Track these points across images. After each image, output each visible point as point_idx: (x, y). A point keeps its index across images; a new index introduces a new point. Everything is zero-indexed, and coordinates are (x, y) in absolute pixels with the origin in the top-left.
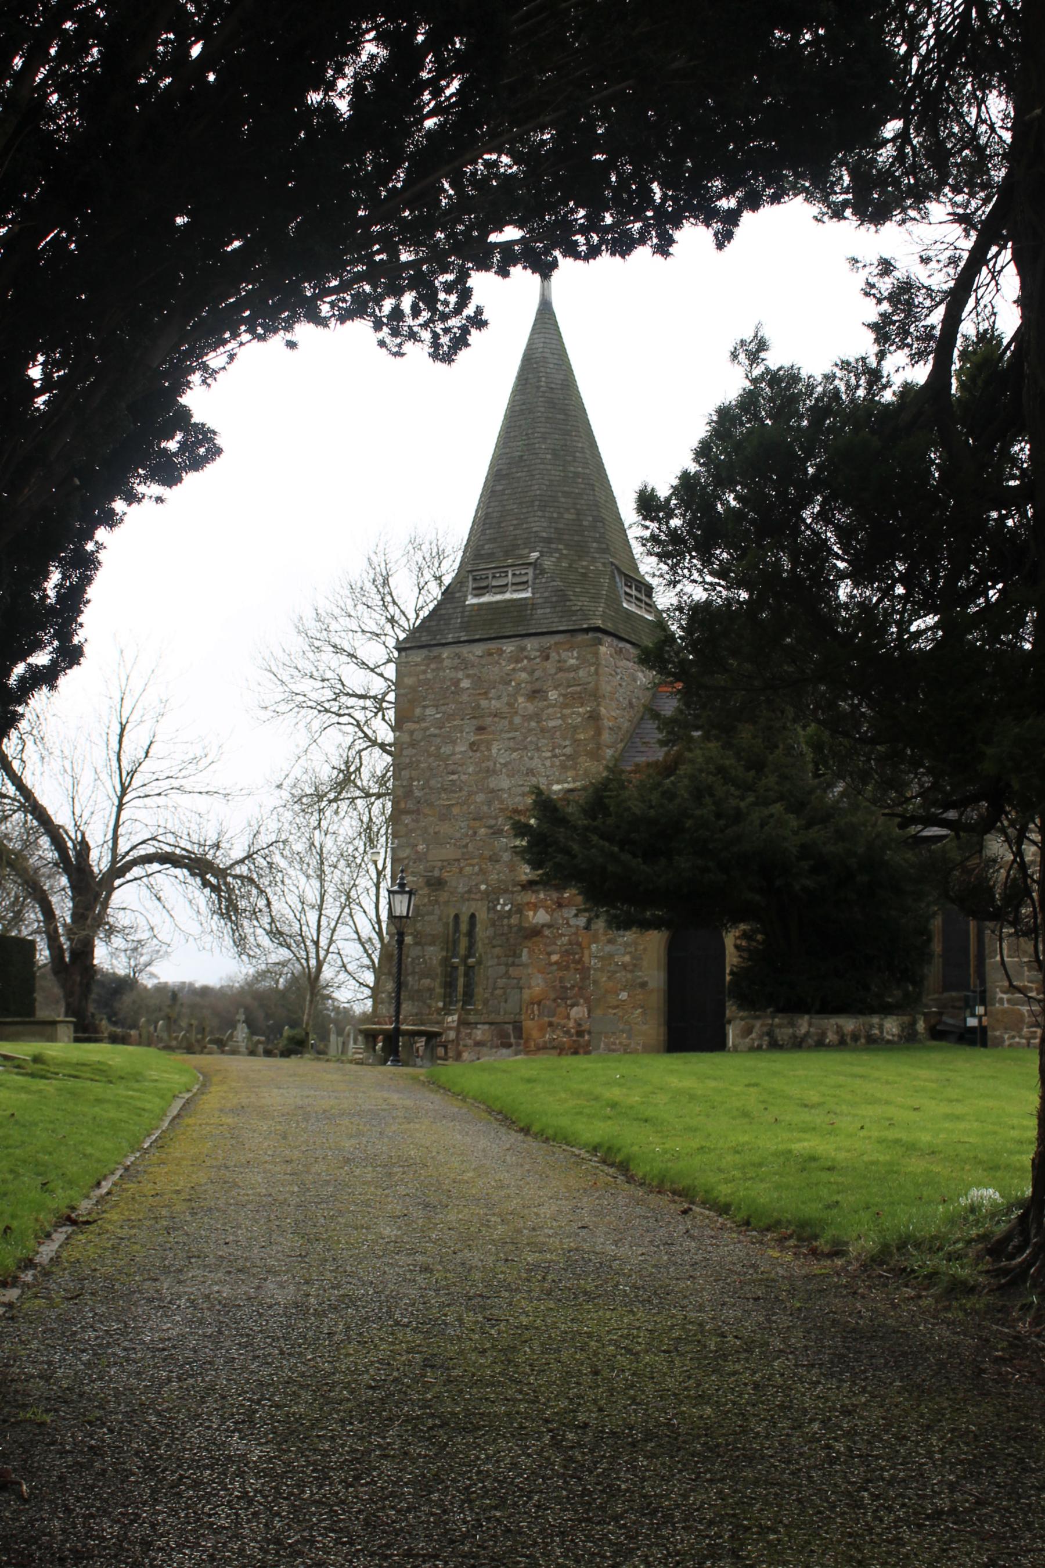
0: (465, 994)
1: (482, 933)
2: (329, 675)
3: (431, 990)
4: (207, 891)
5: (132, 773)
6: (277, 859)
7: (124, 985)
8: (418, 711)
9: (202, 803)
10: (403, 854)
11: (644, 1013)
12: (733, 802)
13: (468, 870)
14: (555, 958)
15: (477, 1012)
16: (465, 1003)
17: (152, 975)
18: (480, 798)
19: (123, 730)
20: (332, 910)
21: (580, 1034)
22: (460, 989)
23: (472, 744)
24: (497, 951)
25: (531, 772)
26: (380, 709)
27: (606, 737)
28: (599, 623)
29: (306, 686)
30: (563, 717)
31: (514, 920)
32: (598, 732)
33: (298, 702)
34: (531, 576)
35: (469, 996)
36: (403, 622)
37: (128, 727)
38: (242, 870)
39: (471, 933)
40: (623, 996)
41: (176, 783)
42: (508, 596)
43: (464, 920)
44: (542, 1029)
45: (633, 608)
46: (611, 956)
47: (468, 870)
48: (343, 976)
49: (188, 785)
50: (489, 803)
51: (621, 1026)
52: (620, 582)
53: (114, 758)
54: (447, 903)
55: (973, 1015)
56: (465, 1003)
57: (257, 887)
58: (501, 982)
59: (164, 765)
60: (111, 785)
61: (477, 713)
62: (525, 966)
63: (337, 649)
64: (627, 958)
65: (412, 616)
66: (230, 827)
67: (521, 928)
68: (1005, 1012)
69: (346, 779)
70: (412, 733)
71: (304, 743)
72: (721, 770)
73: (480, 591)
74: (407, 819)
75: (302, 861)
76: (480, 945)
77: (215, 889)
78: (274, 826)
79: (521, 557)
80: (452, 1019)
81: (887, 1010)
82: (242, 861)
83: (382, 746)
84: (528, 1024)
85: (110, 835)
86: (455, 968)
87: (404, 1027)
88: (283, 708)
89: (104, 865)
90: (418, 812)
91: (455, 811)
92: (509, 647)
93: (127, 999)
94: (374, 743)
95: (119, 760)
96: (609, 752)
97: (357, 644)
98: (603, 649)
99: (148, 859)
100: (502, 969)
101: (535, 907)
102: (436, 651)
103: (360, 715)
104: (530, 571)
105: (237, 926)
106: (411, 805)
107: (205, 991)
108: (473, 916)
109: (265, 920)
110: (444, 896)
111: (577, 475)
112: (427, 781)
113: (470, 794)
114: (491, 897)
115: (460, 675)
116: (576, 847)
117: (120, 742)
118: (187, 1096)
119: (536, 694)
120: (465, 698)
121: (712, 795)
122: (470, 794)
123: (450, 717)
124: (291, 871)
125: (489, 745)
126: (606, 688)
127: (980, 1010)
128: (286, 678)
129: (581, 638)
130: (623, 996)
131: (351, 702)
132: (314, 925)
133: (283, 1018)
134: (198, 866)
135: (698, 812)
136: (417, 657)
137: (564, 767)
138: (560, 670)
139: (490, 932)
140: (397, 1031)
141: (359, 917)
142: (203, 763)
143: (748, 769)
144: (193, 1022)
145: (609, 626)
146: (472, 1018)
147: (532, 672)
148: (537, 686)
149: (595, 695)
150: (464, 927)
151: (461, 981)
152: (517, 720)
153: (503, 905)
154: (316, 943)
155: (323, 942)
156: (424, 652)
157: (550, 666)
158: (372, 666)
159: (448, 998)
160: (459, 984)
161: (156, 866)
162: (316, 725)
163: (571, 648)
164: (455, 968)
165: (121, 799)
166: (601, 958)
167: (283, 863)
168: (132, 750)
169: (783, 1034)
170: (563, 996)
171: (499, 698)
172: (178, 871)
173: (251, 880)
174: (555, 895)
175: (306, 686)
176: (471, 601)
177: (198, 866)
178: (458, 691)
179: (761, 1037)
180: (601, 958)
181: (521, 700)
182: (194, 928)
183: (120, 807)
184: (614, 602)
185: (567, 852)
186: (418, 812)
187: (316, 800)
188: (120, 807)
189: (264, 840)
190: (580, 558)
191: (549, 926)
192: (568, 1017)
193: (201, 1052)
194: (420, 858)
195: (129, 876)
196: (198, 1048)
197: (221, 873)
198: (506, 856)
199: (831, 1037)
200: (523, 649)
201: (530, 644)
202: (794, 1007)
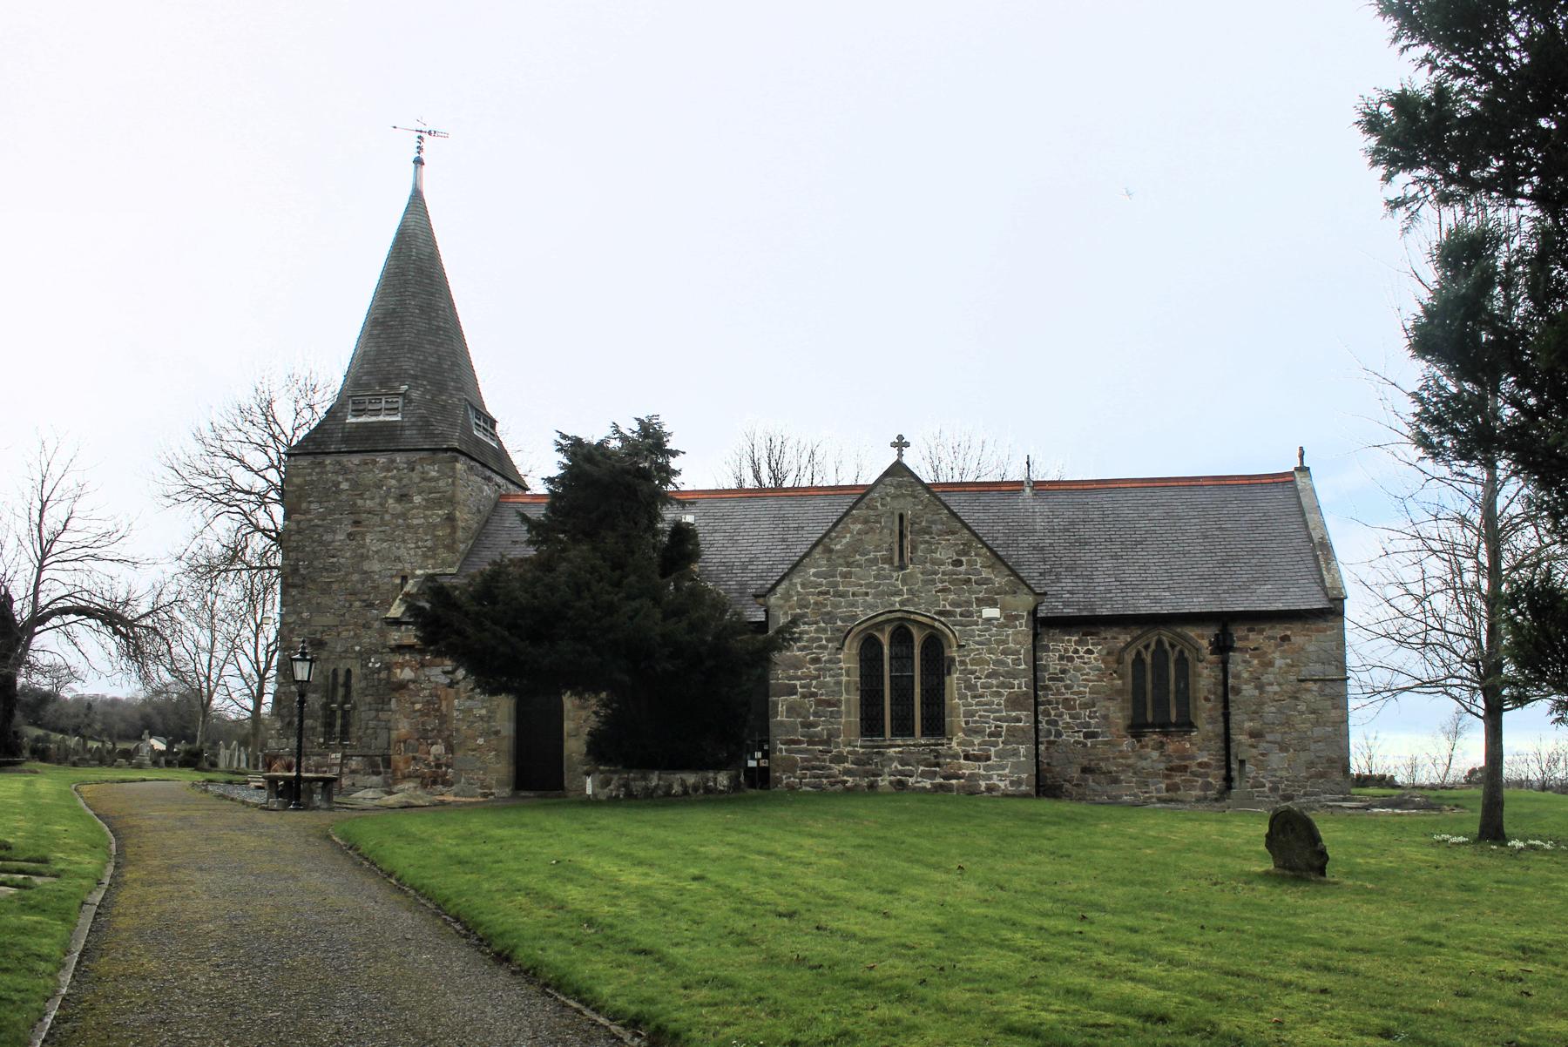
0: (342, 732)
1: (356, 684)
2: (222, 474)
3: (313, 729)
4: (117, 638)
5: (52, 542)
6: (176, 613)
7: (46, 699)
8: (304, 506)
9: (114, 568)
10: (289, 620)
11: (497, 756)
12: (606, 597)
13: (345, 634)
14: (418, 706)
15: (352, 746)
16: (342, 739)
17: (72, 690)
18: (356, 577)
19: (44, 505)
20: (221, 654)
21: (438, 766)
22: (338, 729)
23: (349, 535)
24: (368, 699)
25: (398, 559)
26: (264, 503)
27: (460, 534)
28: (456, 445)
29: (202, 481)
30: (425, 517)
31: (383, 675)
32: (454, 529)
33: (200, 494)
34: (400, 404)
35: (345, 734)
36: (282, 437)
37: (49, 504)
38: (148, 622)
39: (347, 685)
40: (481, 741)
41: (91, 552)
42: (381, 418)
43: (341, 673)
44: (407, 762)
45: (481, 436)
46: (470, 710)
47: (345, 634)
48: (228, 702)
49: (101, 553)
50: (363, 582)
51: (478, 764)
52: (472, 415)
53: (35, 530)
54: (327, 660)
55: (753, 758)
56: (342, 739)
57: (161, 637)
58: (372, 724)
59: (79, 536)
60: (31, 550)
61: (354, 510)
62: (394, 712)
63: (231, 457)
64: (484, 712)
65: (290, 433)
66: (137, 584)
67: (388, 681)
68: (783, 759)
69: (234, 555)
70: (298, 522)
71: (200, 526)
72: (593, 569)
73: (358, 412)
74: (294, 592)
75: (197, 616)
76: (354, 694)
77: (125, 636)
78: (173, 588)
79: (392, 388)
80: (336, 757)
81: (718, 767)
82: (147, 615)
83: (263, 531)
84: (395, 758)
85: (31, 591)
86: (333, 712)
87: (304, 775)
88: (183, 497)
89: (26, 614)
90: (303, 586)
91: (335, 586)
92: (382, 459)
93: (51, 708)
94: (257, 528)
95: (40, 531)
96: (462, 546)
97: (244, 452)
98: (458, 466)
99: (66, 611)
100: (373, 714)
101: (402, 666)
102: (320, 459)
103: (245, 507)
104: (400, 400)
105: (143, 665)
106: (297, 580)
107: (115, 702)
108: (349, 671)
109: (167, 660)
110: (324, 655)
111: (439, 328)
112: (311, 563)
113: (347, 574)
114: (364, 657)
115: (340, 478)
116: (470, 630)
117: (41, 516)
118: (97, 897)
119: (403, 497)
120: (344, 497)
121: (589, 590)
122: (347, 574)
123: (331, 512)
124: (189, 624)
125: (363, 535)
126: (461, 496)
127: (758, 755)
128: (185, 474)
129: (441, 455)
130: (481, 741)
131: (239, 496)
132: (206, 664)
133: (180, 730)
134: (110, 617)
135: (578, 604)
136: (304, 462)
137: (425, 556)
138: (424, 479)
139: (363, 684)
140: (298, 778)
141: (242, 659)
142: (114, 537)
143: (613, 570)
144: (103, 735)
145: (464, 448)
146: (348, 752)
147: (400, 480)
148: (405, 491)
149: (452, 501)
150: (341, 679)
151: (339, 722)
152: (387, 517)
153: (375, 663)
154: (208, 678)
155: (213, 677)
156: (310, 459)
157: (415, 476)
158: (259, 471)
159: (328, 735)
160: (337, 726)
161: (72, 617)
162: (210, 512)
163: (433, 463)
164: (333, 712)
165: (41, 562)
166: (462, 711)
167: (181, 617)
168: (52, 521)
169: (637, 786)
170: (424, 736)
171: (372, 498)
172: (92, 622)
173: (155, 629)
174: (419, 657)
175: (202, 481)
176: (351, 420)
177: (110, 617)
178: (339, 492)
179: (618, 788)
180: (462, 711)
181: (390, 501)
182: (107, 668)
183: (41, 569)
184: (467, 429)
185: (459, 633)
186: (303, 586)
187: (209, 571)
188: (41, 569)
189: (165, 599)
190: (441, 393)
191: (414, 682)
192: (428, 753)
193: (111, 765)
194: (304, 623)
195: (48, 625)
196: (108, 760)
197: (130, 624)
198: (377, 625)
199: (676, 789)
200: (393, 461)
201: (399, 458)
202: (647, 764)
